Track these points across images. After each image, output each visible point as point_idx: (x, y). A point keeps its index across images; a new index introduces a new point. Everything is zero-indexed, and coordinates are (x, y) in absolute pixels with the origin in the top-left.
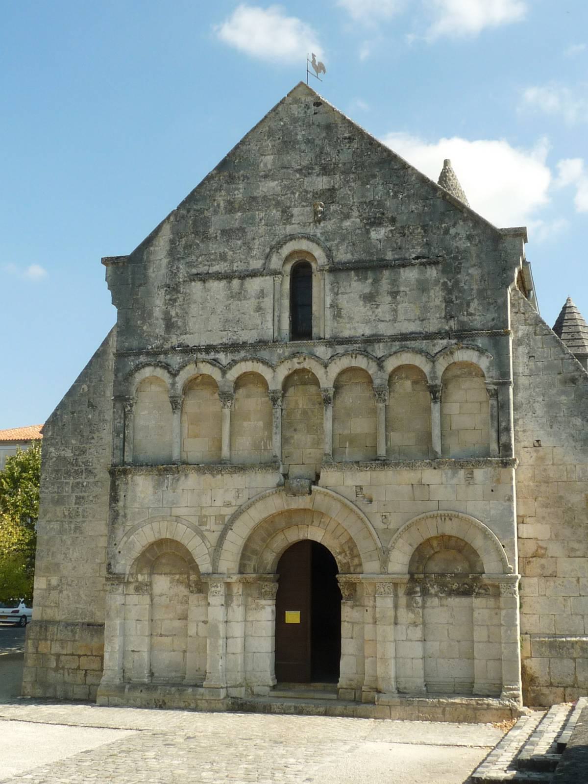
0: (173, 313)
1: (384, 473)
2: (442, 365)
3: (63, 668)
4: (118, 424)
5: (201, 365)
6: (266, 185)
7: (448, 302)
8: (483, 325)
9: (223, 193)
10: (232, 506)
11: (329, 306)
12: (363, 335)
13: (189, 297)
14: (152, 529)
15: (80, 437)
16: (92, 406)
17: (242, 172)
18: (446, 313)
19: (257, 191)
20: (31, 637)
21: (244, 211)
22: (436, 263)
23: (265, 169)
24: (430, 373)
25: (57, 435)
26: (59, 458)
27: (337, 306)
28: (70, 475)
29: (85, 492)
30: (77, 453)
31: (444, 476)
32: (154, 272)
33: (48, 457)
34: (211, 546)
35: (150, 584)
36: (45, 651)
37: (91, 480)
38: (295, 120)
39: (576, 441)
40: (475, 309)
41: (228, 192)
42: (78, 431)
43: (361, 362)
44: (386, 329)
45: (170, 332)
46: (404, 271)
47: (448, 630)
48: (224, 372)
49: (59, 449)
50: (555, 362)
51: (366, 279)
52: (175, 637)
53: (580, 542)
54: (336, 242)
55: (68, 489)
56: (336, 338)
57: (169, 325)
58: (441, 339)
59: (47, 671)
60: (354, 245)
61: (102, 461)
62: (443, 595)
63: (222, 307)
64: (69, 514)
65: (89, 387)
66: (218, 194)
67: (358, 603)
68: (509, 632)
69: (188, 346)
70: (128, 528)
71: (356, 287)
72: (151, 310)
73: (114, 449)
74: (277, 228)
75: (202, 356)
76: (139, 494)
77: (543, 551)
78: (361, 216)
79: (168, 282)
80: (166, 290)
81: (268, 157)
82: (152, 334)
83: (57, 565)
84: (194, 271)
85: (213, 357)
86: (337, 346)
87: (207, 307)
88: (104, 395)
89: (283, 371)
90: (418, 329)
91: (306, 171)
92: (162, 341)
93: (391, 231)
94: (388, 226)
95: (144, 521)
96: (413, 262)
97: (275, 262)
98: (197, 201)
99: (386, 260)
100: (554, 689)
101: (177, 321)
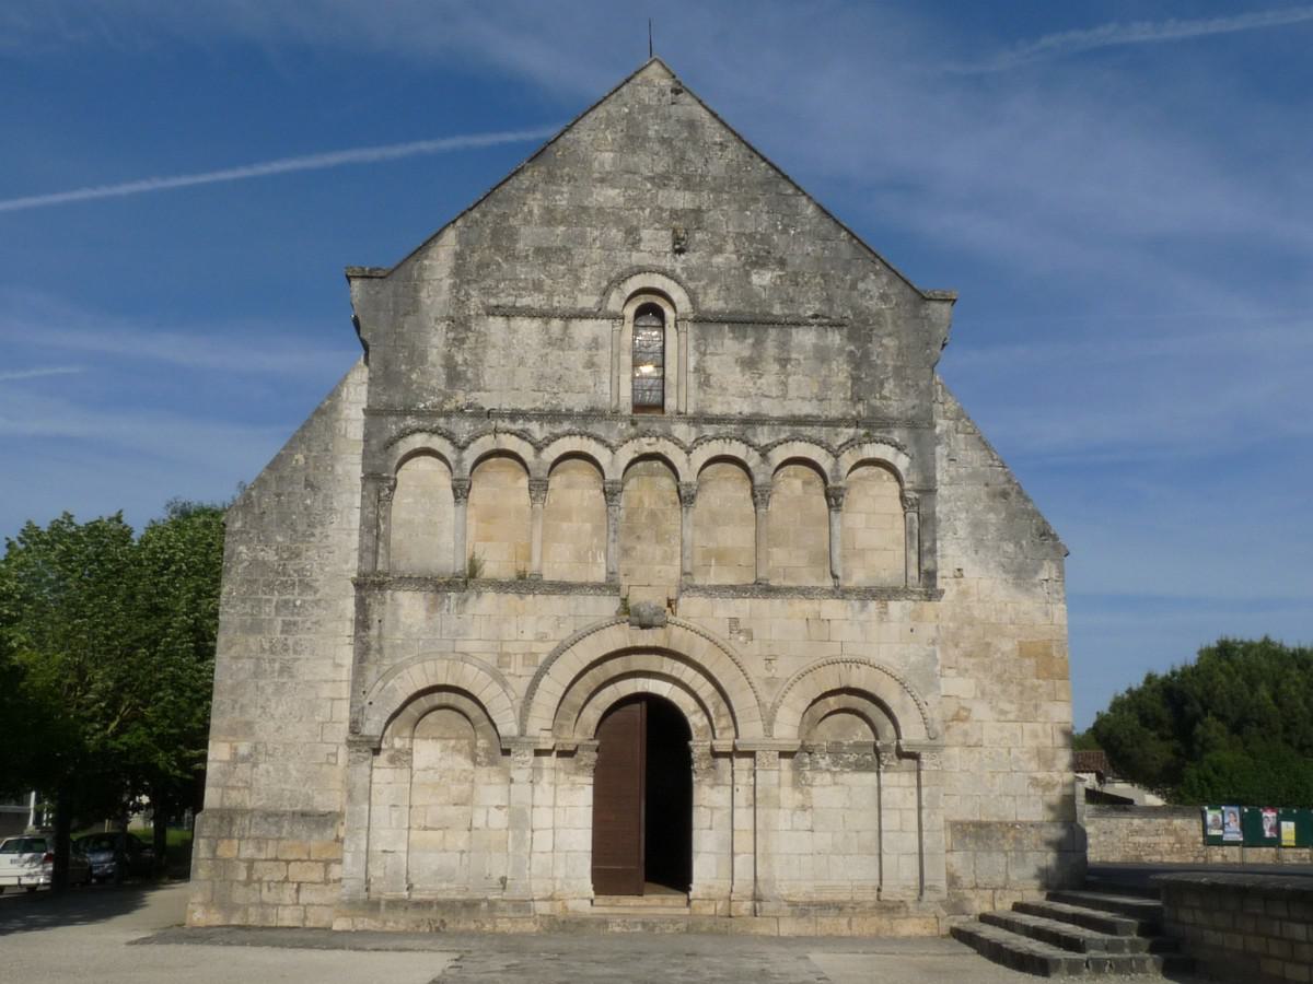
0: (459, 359)
1: (768, 601)
2: (848, 459)
3: (260, 881)
4: (370, 515)
5: (502, 437)
6: (603, 193)
7: (856, 379)
8: (901, 413)
9: (538, 196)
10: (549, 641)
11: (692, 370)
12: (740, 413)
13: (483, 339)
14: (424, 670)
15: (290, 532)
16: (312, 486)
17: (566, 170)
18: (853, 394)
19: (590, 199)
20: (205, 834)
21: (569, 225)
22: (840, 325)
23: (601, 170)
24: (832, 470)
25: (251, 527)
26: (255, 562)
27: (704, 371)
28: (273, 589)
29: (298, 614)
30: (285, 556)
31: (849, 608)
32: (429, 296)
33: (234, 559)
34: (517, 697)
35: (410, 753)
36: (228, 855)
37: (309, 598)
38: (645, 108)
39: (1006, 571)
40: (891, 392)
41: (546, 195)
42: (288, 522)
43: (737, 450)
44: (772, 409)
45: (455, 385)
46: (797, 333)
47: (844, 817)
48: (538, 449)
49: (254, 549)
50: (982, 469)
51: (745, 337)
52: (447, 831)
53: (1012, 702)
54: (703, 283)
55: (269, 609)
56: (703, 413)
57: (454, 376)
58: (847, 427)
59: (231, 885)
60: (728, 289)
61: (327, 569)
62: (838, 769)
63: (536, 357)
64: (271, 648)
65: (306, 458)
66: (530, 196)
67: (719, 782)
68: (933, 817)
69: (482, 408)
70: (386, 668)
71: (730, 346)
72: (425, 351)
73: (363, 551)
74: (619, 254)
75: (505, 424)
76: (403, 619)
77: (965, 714)
78: (738, 251)
79: (451, 313)
80: (449, 325)
81: (607, 154)
82: (426, 386)
83: (249, 725)
84: (493, 302)
85: (520, 427)
86: (704, 426)
87: (512, 355)
88: (332, 472)
89: (627, 453)
90: (815, 412)
91: (661, 181)
92: (441, 398)
93: (780, 277)
94: (774, 270)
95: (412, 659)
96: (811, 321)
97: (615, 302)
98: (499, 201)
99: (772, 315)
100: (982, 892)
101: (465, 372)
